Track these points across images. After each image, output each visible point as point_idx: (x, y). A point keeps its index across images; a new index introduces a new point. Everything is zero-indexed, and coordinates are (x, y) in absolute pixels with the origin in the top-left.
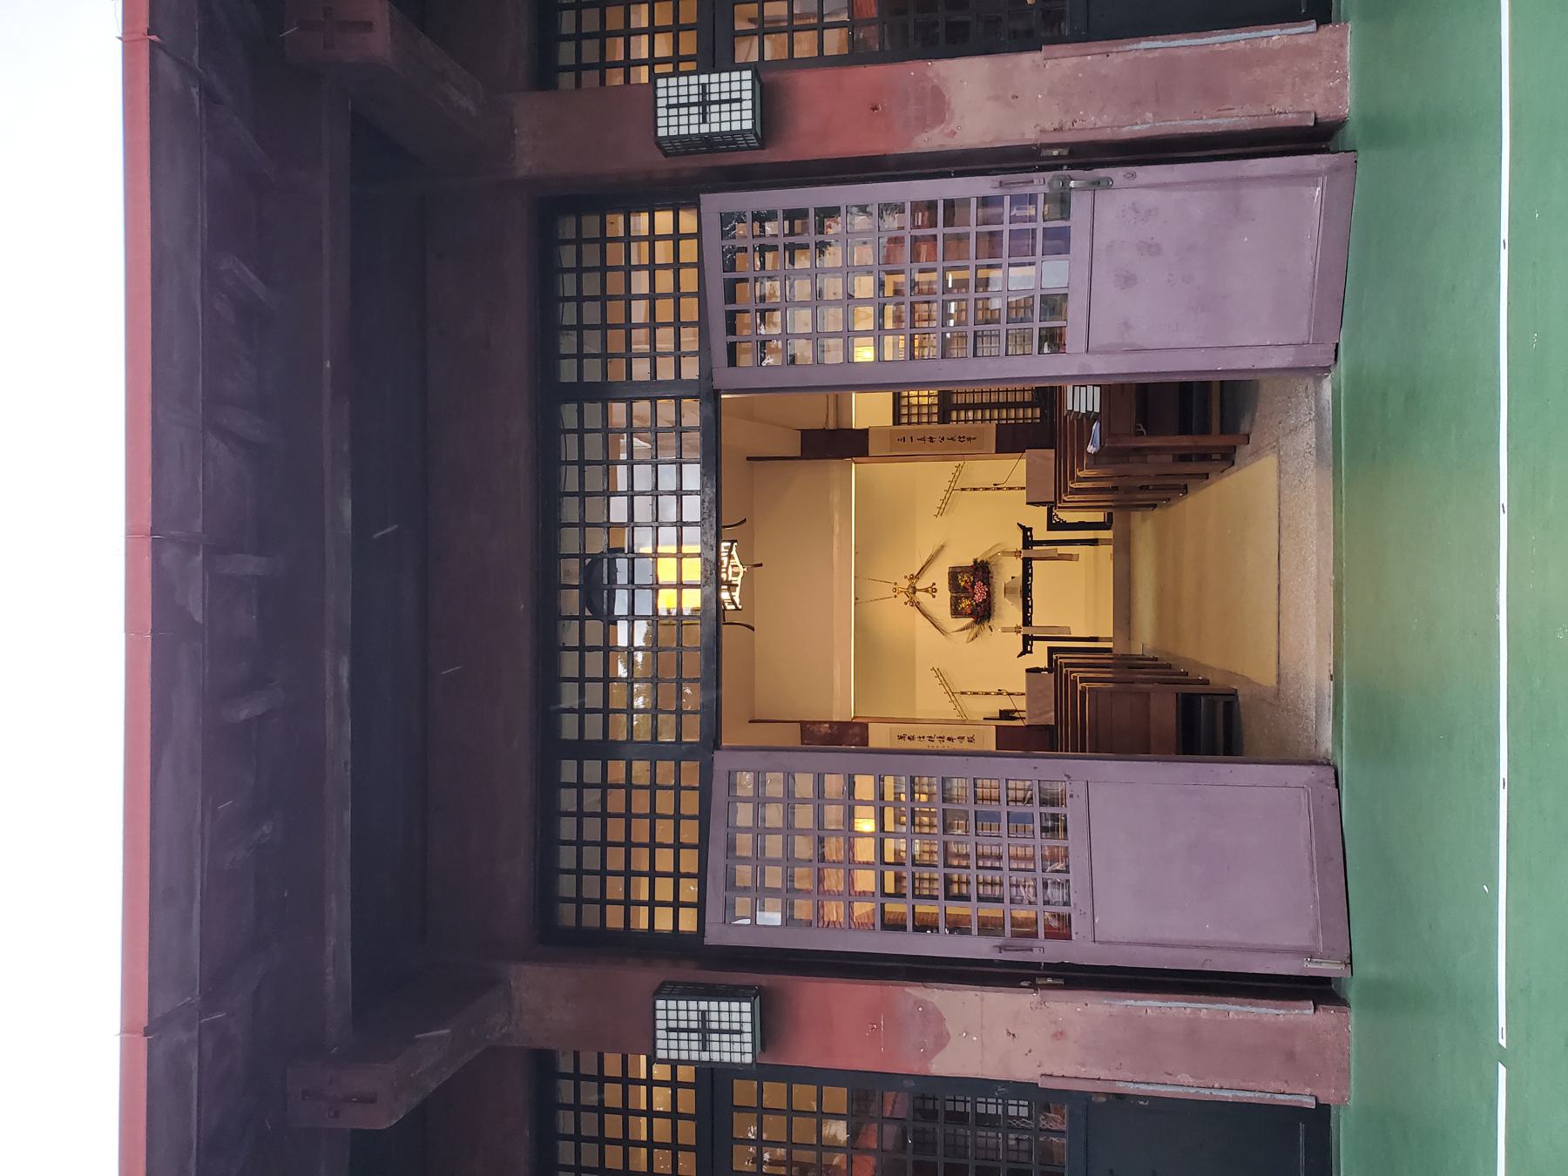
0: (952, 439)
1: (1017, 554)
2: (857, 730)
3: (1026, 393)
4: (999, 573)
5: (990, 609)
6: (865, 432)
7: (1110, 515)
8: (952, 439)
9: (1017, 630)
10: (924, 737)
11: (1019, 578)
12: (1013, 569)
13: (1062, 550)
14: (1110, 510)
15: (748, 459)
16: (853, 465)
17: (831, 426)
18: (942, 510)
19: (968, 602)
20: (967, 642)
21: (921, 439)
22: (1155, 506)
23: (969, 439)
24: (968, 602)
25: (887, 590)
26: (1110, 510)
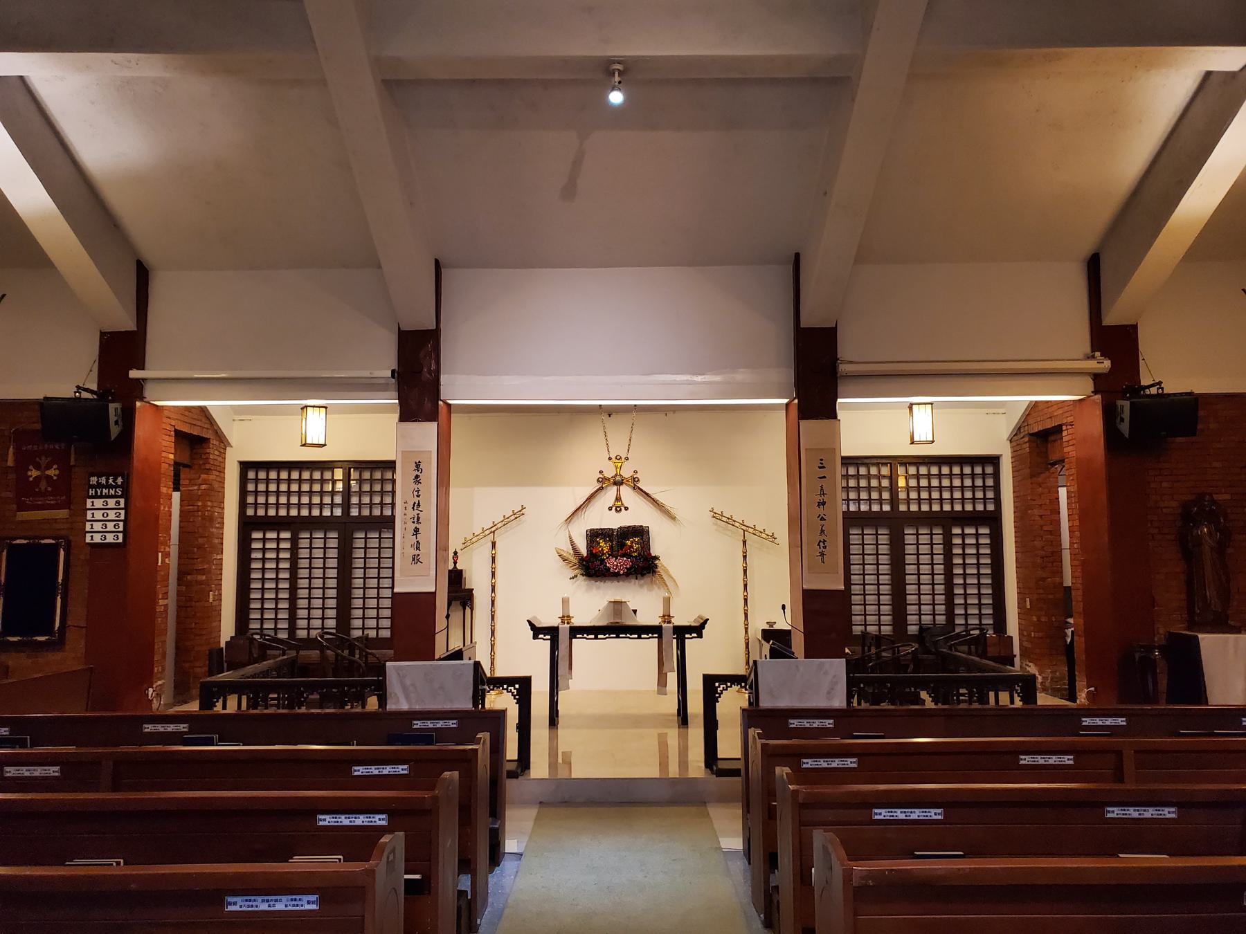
0: (822, 531)
1: (667, 617)
2: (428, 405)
3: (877, 627)
4: (641, 586)
5: (597, 576)
6: (833, 415)
7: (734, 773)
8: (822, 531)
9: (566, 618)
10: (418, 496)
11: (635, 620)
12: (648, 614)
13: (672, 678)
14: (743, 772)
15: (797, 256)
16: (785, 401)
17: (843, 368)
18: (718, 517)
19: (606, 550)
20: (556, 548)
21: (822, 490)
22: (749, 863)
23: (822, 554)
24: (606, 550)
25: (618, 449)
26: (743, 772)
